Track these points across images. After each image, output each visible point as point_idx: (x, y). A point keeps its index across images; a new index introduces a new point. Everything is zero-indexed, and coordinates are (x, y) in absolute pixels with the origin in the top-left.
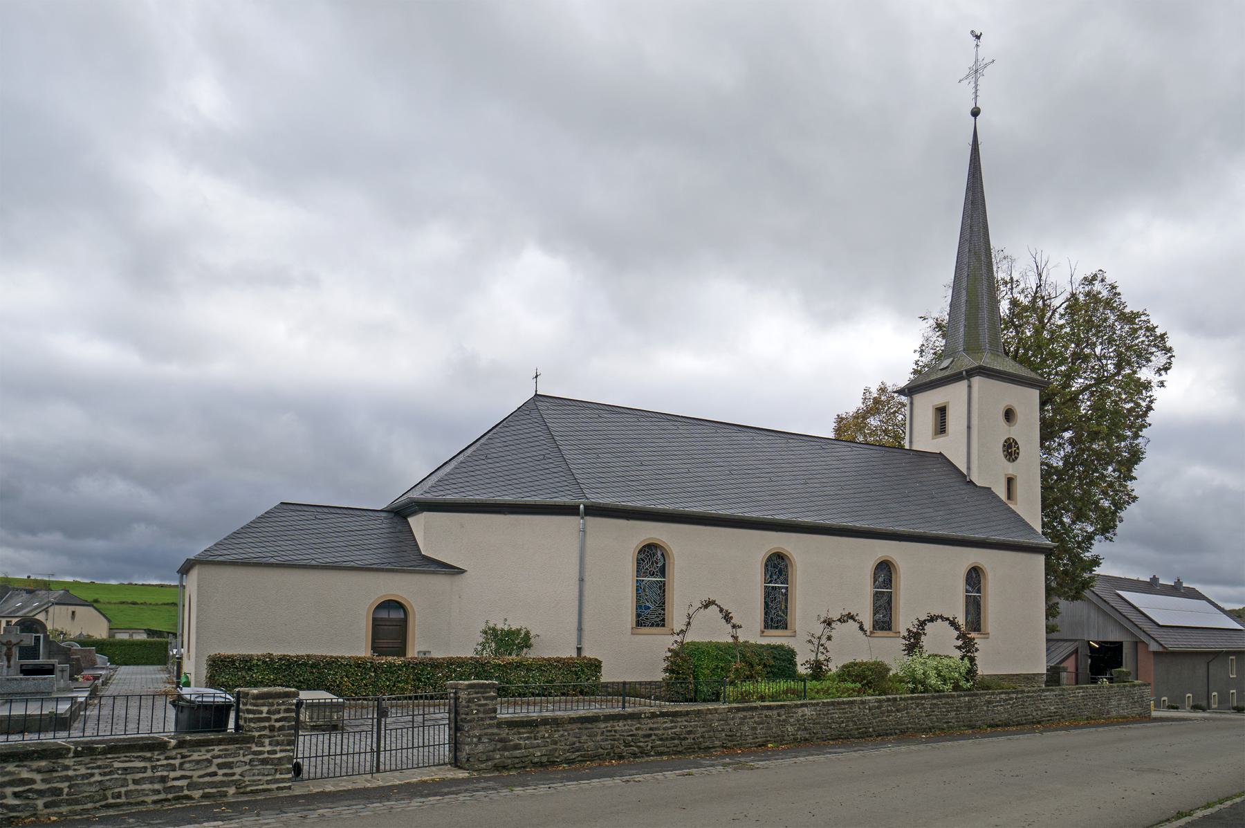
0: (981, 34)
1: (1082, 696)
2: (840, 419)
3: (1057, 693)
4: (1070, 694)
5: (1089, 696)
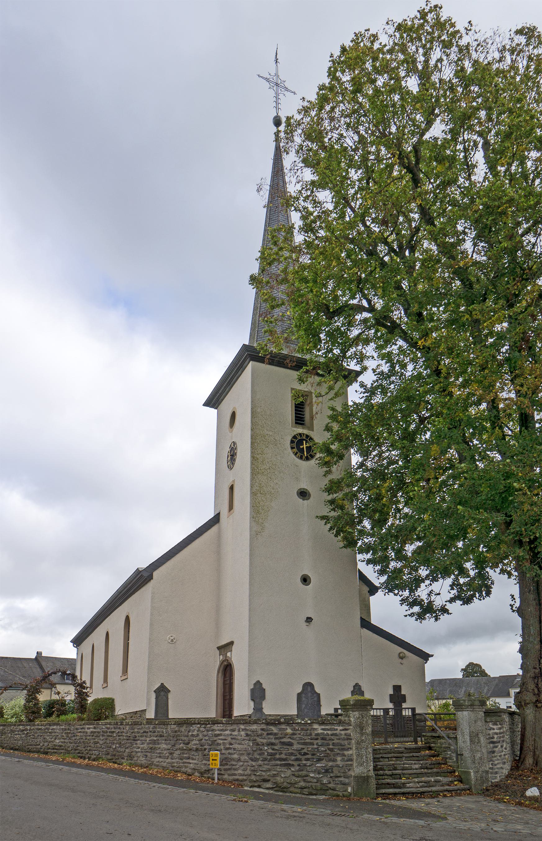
0: (451, 614)
1: (92, 732)
2: (253, 279)
3: (63, 727)
4: (77, 729)
5: (101, 733)
